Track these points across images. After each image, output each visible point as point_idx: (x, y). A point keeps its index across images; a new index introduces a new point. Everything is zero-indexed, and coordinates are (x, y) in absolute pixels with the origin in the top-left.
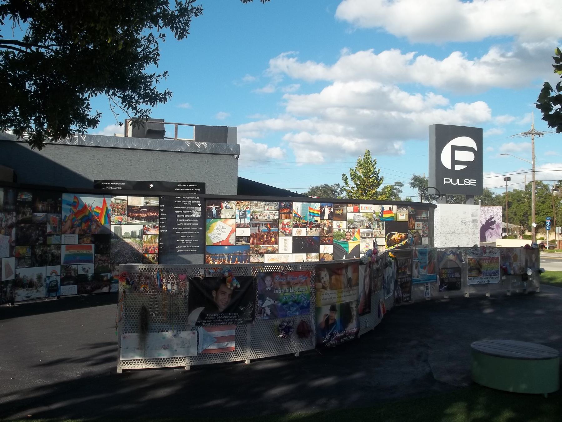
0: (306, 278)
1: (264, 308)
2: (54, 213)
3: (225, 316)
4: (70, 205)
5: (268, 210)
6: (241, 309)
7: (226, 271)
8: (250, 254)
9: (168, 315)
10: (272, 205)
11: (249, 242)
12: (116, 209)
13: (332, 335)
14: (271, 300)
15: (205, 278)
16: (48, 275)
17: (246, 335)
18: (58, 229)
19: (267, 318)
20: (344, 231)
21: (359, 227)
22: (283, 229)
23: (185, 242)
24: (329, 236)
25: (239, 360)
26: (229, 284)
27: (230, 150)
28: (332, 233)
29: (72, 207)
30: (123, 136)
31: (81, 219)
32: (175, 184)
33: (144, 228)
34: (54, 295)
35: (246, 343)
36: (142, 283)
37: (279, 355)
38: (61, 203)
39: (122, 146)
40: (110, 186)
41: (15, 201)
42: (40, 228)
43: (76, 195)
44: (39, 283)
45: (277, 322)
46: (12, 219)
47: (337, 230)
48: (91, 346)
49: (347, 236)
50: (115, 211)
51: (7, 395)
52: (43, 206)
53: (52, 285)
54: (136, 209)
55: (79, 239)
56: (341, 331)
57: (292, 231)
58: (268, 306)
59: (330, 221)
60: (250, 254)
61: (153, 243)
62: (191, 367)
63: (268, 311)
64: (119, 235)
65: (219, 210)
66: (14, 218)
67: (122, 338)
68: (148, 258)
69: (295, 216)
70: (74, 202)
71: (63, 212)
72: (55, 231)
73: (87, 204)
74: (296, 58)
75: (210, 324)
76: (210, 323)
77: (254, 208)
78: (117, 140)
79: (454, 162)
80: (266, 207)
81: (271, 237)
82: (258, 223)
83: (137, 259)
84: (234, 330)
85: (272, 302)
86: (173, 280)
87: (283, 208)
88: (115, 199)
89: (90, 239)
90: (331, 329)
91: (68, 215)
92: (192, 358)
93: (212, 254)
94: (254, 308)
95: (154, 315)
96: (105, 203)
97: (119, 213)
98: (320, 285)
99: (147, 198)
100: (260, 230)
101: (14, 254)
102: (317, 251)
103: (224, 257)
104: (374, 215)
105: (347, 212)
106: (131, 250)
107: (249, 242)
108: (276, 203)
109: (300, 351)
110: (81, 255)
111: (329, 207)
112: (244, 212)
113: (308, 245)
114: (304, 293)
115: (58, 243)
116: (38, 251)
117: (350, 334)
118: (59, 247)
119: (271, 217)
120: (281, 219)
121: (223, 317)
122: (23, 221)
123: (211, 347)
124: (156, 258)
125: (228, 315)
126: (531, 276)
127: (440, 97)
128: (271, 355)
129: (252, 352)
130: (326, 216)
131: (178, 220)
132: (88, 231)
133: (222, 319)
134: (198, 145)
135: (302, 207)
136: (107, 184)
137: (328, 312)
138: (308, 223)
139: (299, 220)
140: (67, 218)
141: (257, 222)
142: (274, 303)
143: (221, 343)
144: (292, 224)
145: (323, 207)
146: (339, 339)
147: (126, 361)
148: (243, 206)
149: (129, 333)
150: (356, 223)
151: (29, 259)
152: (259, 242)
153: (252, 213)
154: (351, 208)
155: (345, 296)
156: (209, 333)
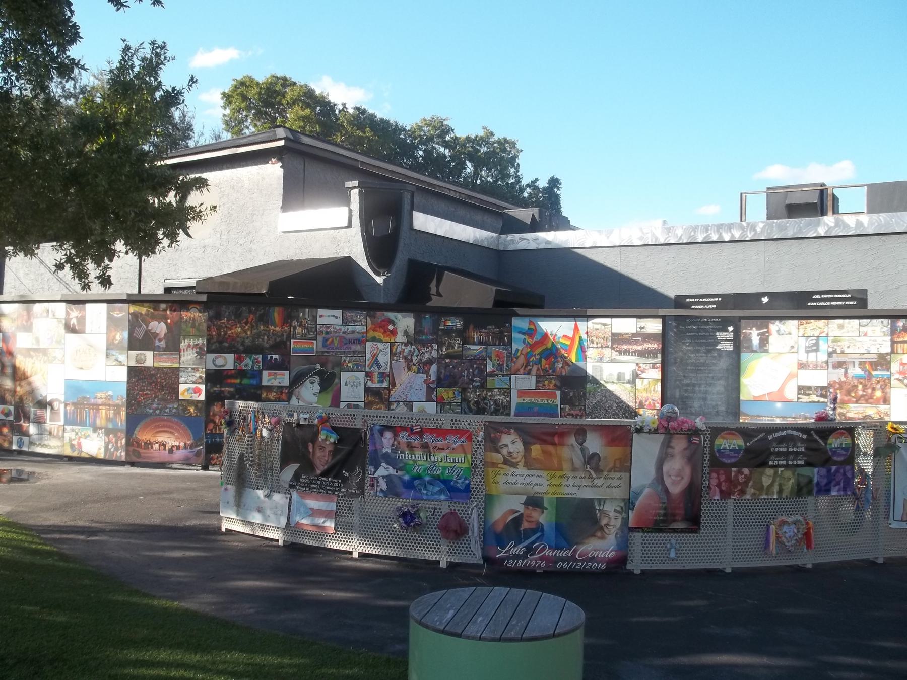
2: (499, 345)
4: (524, 334)
5: (865, 335)
11: (825, 396)
12: (595, 339)
13: (530, 550)
15: (298, 425)
18: (505, 367)
22: (900, 373)
29: (526, 337)
33: (637, 367)
37: (405, 556)
38: (510, 331)
40: (698, 303)
41: (436, 330)
42: (475, 366)
43: (533, 319)
50: (592, 342)
54: (625, 339)
55: (537, 382)
58: (384, 477)
61: (652, 392)
63: (383, 485)
64: (598, 378)
71: (513, 344)
72: (501, 370)
73: (549, 333)
77: (838, 333)
78: (707, 230)
80: (862, 329)
81: (874, 389)
82: (845, 362)
84: (335, 505)
87: (901, 331)
88: (593, 323)
89: (553, 382)
90: (526, 538)
91: (520, 348)
96: (576, 329)
97: (599, 345)
99: (642, 320)
100: (850, 375)
106: (617, 401)
108: (886, 321)
110: (541, 405)
112: (814, 341)
114: (457, 465)
116: (472, 397)
117: (592, 559)
118: (507, 392)
119: (874, 350)
120: (897, 353)
121: (321, 481)
122: (448, 356)
123: (304, 521)
132: (551, 371)
133: (321, 485)
136: (693, 300)
137: (521, 509)
141: (842, 359)
148: (814, 329)
152: (846, 398)
153: (833, 341)
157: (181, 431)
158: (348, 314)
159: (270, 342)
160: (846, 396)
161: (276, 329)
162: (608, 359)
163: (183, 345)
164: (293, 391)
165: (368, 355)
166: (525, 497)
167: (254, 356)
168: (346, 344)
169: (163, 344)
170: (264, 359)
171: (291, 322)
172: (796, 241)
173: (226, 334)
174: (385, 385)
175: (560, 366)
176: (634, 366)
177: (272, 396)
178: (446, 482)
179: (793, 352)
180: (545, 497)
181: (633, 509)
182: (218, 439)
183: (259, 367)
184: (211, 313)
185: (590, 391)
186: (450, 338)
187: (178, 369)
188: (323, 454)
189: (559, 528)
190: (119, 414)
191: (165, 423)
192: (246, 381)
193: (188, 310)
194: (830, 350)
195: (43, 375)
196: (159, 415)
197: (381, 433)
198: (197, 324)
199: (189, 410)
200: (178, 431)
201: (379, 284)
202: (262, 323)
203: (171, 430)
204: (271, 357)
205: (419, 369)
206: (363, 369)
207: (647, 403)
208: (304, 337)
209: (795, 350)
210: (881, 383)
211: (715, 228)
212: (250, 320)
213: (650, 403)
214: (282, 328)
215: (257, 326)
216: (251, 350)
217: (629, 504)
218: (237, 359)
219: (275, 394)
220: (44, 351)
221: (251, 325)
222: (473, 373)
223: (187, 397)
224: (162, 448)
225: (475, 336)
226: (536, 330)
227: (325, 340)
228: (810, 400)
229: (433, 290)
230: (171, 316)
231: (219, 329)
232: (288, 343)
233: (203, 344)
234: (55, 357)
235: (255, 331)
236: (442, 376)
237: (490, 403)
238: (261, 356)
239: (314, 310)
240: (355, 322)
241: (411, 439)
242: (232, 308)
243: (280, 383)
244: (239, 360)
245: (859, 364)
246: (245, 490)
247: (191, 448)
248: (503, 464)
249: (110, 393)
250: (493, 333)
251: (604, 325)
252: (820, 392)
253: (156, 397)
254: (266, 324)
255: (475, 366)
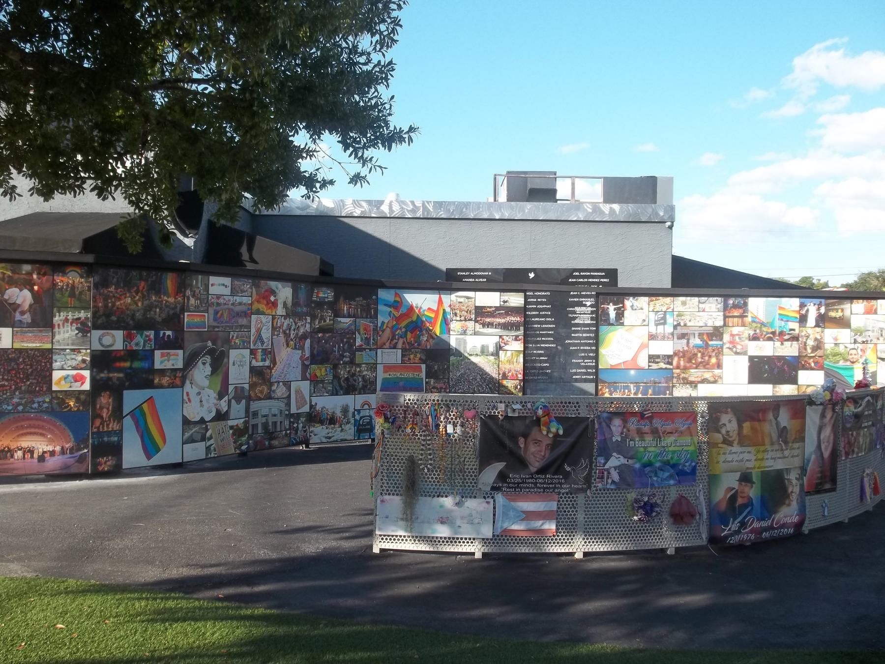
0: (690, 424)
1: (608, 470)
2: (367, 317)
3: (541, 479)
4: (390, 306)
5: (704, 311)
6: (568, 469)
7: (540, 406)
8: (673, 383)
9: (449, 472)
10: (711, 303)
11: (671, 364)
12: (458, 312)
13: (743, 524)
14: (622, 457)
15: (507, 418)
16: (358, 407)
17: (577, 511)
19: (613, 487)
20: (846, 347)
21: (875, 341)
22: (731, 342)
23: (585, 363)
24: (816, 356)
25: (563, 551)
26: (544, 428)
27: (657, 214)
28: (822, 351)
29: (392, 310)
30: (491, 200)
31: (406, 327)
32: (570, 273)
33: (501, 340)
34: (367, 437)
35: (576, 525)
36: (409, 421)
37: (635, 548)
38: (376, 303)
39: (485, 216)
41: (309, 301)
42: (345, 340)
43: (398, 291)
44: (344, 418)
45: (632, 496)
46: (305, 327)
47: (833, 345)
48: (365, 512)
49: (850, 357)
50: (456, 315)
51: (212, 566)
52: (350, 308)
53: (363, 422)
54: (488, 312)
55: (403, 356)
56: (762, 519)
57: (747, 346)
58: (615, 468)
60: (673, 383)
61: (515, 363)
62: (484, 554)
63: (615, 476)
65: (621, 312)
66: (308, 326)
67: (378, 501)
68: (506, 387)
69: (753, 322)
70: (395, 301)
72: (368, 344)
73: (414, 305)
74: (842, 50)
75: (515, 490)
76: (515, 488)
77: (681, 309)
78: (479, 208)
80: (701, 306)
81: (710, 357)
82: (687, 334)
83: (490, 388)
84: (555, 503)
85: (623, 461)
86: (456, 419)
87: (732, 307)
88: (457, 296)
89: (418, 356)
90: (740, 514)
91: (386, 321)
92: (485, 541)
93: (609, 383)
94: (591, 469)
95: (426, 470)
96: (440, 301)
97: (462, 318)
98: (718, 437)
99: (505, 294)
100: (691, 345)
101: (308, 376)
102: (794, 381)
103: (628, 387)
105: (851, 314)
106: (481, 373)
107: (671, 364)
108: (719, 299)
109: (677, 546)
111: (817, 306)
112: (662, 315)
113: (776, 370)
114: (685, 448)
115: (373, 361)
116: (343, 373)
117: (783, 526)
118: (373, 367)
119: (710, 323)
121: (536, 479)
122: (321, 330)
123: (515, 527)
124: (519, 387)
125: (545, 478)
128: (621, 548)
129: (585, 540)
131: (573, 329)
132: (416, 344)
133: (535, 484)
134: (606, 208)
137: (736, 485)
138: (777, 333)
139: (761, 328)
140: (385, 325)
142: (627, 463)
143: (533, 522)
144: (747, 336)
145: (806, 306)
146: (758, 532)
147: (385, 536)
148: (662, 305)
149: (389, 494)
150: (870, 333)
151: (330, 383)
152: (688, 365)
153: (678, 316)
154: (859, 306)
155: (772, 459)
156: (513, 503)
157: (57, 432)
158: (236, 283)
159: (164, 315)
160: (688, 362)
161: (170, 299)
162: (472, 332)
163: (57, 319)
164: (186, 374)
165: (253, 330)
166: (739, 473)
167: (146, 333)
168: (234, 317)
169: (27, 318)
170: (157, 335)
171: (185, 292)
173: (114, 305)
174: (267, 363)
175: (425, 339)
176: (497, 339)
177: (165, 381)
178: (674, 466)
179: (644, 325)
180: (754, 472)
181: (805, 476)
182: (106, 439)
183: (151, 347)
184: (97, 278)
185: (453, 364)
186: (322, 311)
187: (50, 351)
188: (538, 448)
189: (763, 501)
191: (32, 422)
192: (137, 364)
193: (64, 273)
194: (675, 323)
196: (22, 412)
197: (610, 419)
198: (77, 293)
199: (68, 403)
200: (52, 432)
201: (188, 247)
202: (154, 292)
203: (41, 431)
204: (164, 334)
205: (295, 345)
206: (248, 346)
207: (510, 374)
208: (197, 309)
209: (646, 323)
210: (716, 351)
211: (487, 206)
212: (141, 288)
213: (512, 373)
214: (176, 299)
215: (148, 296)
216: (142, 325)
217: (803, 469)
218: (127, 337)
219: (168, 379)
221: (143, 294)
222: (343, 347)
223: (65, 387)
224: (28, 455)
225: (345, 309)
226: (402, 302)
227: (216, 313)
228: (659, 367)
229: (245, 256)
230: (40, 281)
231: (106, 299)
232: (182, 316)
233: (87, 318)
235: (146, 302)
236: (315, 352)
237: (358, 379)
238: (153, 332)
239: (206, 277)
240: (242, 291)
241: (641, 425)
242: (121, 272)
243: (173, 365)
244: (128, 338)
245: (699, 336)
246: (418, 499)
247: (71, 453)
248: (722, 443)
250: (361, 305)
251: (468, 298)
252: (667, 360)
253: (20, 388)
254: (158, 293)
255: (345, 340)
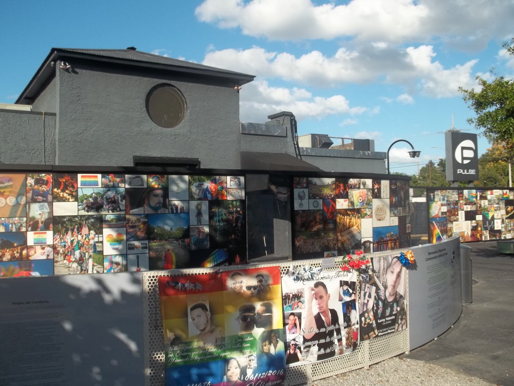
59: (480, 200)
77: (448, 194)
79: (463, 158)
102: (475, 219)
104: (500, 196)
107: (446, 215)
126: (3, 273)
127: (303, 91)
130: (478, 198)
135: (468, 192)
141: (449, 203)
154: (489, 192)
172: (250, 136)
190: (396, 244)
195: (358, 227)
220: (358, 211)
234: (366, 214)
249: (392, 233)
